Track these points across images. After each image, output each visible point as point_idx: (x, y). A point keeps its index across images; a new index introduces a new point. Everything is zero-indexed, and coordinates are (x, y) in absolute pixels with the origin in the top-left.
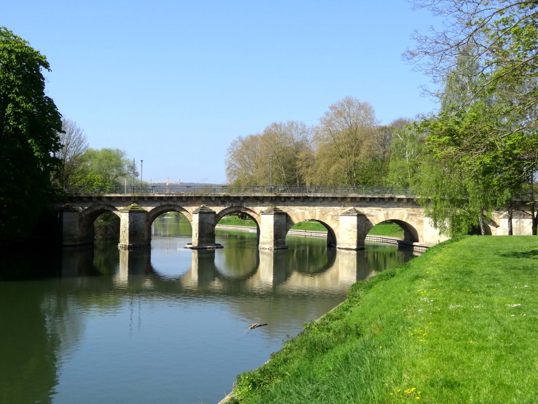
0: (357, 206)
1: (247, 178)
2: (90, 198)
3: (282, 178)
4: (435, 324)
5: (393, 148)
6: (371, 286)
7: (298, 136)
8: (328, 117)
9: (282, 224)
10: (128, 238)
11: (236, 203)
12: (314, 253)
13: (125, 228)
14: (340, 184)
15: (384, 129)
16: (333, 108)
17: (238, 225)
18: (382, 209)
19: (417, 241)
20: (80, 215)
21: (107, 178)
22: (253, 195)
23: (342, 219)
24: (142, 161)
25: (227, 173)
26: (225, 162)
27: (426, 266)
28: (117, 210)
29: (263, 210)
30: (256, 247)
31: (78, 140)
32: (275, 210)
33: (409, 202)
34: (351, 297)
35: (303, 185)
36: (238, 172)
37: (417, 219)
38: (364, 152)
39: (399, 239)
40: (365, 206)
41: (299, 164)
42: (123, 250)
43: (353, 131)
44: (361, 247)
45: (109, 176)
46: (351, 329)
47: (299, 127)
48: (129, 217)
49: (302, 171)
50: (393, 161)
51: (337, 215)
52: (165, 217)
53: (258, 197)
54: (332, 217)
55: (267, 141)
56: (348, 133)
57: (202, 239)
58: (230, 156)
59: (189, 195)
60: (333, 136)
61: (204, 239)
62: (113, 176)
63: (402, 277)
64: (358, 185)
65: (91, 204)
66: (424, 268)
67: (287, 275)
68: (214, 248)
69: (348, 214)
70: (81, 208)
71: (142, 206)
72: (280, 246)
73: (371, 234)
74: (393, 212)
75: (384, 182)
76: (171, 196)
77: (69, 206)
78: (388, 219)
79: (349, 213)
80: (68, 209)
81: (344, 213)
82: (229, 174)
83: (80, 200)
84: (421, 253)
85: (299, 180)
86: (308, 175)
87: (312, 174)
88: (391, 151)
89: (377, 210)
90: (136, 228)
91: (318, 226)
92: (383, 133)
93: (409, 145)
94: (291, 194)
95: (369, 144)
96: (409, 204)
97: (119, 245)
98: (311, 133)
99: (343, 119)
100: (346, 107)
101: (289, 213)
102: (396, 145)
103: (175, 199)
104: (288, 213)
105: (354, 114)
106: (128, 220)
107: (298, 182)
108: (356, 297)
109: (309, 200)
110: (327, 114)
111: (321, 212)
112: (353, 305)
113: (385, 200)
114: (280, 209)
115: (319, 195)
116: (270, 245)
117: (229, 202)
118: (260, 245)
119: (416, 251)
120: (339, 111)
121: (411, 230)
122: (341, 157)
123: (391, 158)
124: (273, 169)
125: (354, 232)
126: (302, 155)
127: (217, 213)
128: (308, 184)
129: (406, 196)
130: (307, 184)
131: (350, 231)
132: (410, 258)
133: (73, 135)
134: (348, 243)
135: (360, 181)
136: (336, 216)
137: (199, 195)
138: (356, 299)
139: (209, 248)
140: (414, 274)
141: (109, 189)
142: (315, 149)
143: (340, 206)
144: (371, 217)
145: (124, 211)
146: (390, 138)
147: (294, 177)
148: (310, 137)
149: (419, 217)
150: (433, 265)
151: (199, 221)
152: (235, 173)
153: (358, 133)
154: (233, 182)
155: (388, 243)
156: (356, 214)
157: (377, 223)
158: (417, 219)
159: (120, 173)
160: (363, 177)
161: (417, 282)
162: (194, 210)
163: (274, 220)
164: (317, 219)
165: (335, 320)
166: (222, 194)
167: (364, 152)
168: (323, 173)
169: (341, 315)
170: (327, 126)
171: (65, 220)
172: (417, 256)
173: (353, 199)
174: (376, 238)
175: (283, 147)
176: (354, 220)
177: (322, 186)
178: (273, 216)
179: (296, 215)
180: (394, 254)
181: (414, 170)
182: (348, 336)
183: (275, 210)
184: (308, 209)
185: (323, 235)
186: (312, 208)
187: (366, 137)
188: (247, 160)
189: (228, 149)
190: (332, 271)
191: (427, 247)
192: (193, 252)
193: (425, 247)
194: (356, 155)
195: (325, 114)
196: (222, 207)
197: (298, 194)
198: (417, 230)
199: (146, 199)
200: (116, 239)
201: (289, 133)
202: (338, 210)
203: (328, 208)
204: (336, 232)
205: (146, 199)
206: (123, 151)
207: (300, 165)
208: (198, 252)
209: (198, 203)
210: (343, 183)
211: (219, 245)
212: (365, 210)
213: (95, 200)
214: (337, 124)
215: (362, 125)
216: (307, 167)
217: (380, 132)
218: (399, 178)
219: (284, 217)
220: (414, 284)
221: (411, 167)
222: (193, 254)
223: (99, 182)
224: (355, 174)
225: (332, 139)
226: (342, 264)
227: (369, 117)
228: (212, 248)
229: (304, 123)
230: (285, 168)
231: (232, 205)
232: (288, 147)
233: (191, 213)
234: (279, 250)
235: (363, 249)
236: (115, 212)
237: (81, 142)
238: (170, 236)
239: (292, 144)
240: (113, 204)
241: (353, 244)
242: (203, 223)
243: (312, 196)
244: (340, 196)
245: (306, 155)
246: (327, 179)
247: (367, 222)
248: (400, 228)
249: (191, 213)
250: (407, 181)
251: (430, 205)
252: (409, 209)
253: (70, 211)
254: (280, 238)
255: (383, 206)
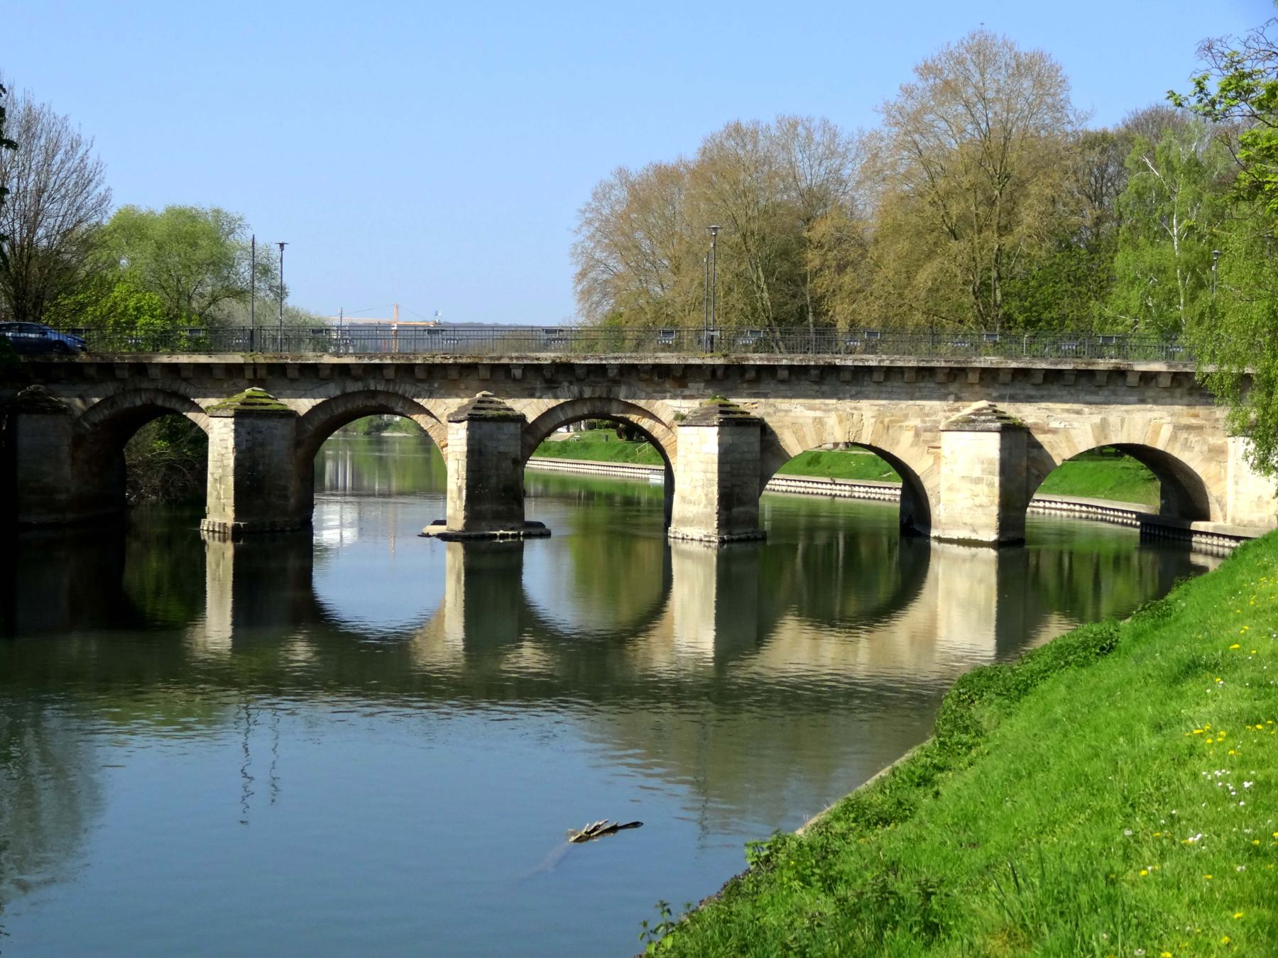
0: (1001, 398)
1: (645, 306)
2: (107, 370)
3: (759, 305)
4: (1260, 923)
5: (1127, 205)
6: (1028, 686)
7: (811, 167)
8: (910, 102)
9: (749, 456)
10: (232, 501)
11: (593, 385)
12: (864, 550)
13: (224, 467)
14: (950, 326)
15: (1100, 142)
16: (927, 70)
17: (612, 459)
18: (1086, 409)
19: (1205, 517)
20: (77, 423)
21: (183, 303)
22: (650, 361)
23: (950, 441)
24: (282, 245)
25: (579, 288)
26: (573, 255)
27: (1231, 616)
28: (198, 409)
29: (685, 412)
30: (661, 534)
31: (74, 176)
32: (725, 409)
33: (1180, 385)
34: (948, 727)
35: (826, 335)
36: (616, 287)
37: (1205, 442)
38: (1030, 220)
39: (1143, 509)
40: (1029, 399)
41: (813, 259)
42: (217, 542)
43: (993, 148)
44: (1012, 535)
45: (190, 298)
46: (901, 906)
47: (817, 137)
48: (236, 431)
49: (822, 284)
50: (1129, 249)
51: (934, 429)
52: (385, 434)
53: (669, 366)
54: (917, 435)
55: (711, 184)
56: (979, 155)
57: (477, 508)
58: (588, 234)
59: (438, 360)
60: (926, 168)
61: (486, 507)
62: (202, 296)
63: (1139, 660)
64: (1010, 328)
65: (110, 388)
66: (1221, 627)
67: (763, 632)
68: (518, 535)
69: (968, 424)
70: (78, 402)
71: (280, 395)
72: (739, 532)
73: (1049, 490)
74: (1123, 421)
75: (1096, 322)
76: (377, 361)
77: (39, 394)
78: (1104, 443)
79: (974, 421)
80: (35, 405)
81: (956, 422)
82: (586, 294)
83: (77, 375)
84: (1217, 556)
85: (815, 314)
86: (844, 294)
87: (858, 292)
88: (1121, 214)
89: (1068, 411)
90: (260, 467)
91: (877, 465)
92: (1094, 156)
93: (1183, 192)
94: (780, 356)
95: (1048, 191)
96: (1178, 392)
97: (205, 524)
98: (857, 155)
99: (961, 109)
100: (972, 67)
101: (771, 422)
102: (1140, 195)
103: (390, 374)
104: (767, 420)
105: (998, 92)
106: (231, 443)
107: (811, 319)
108: (966, 730)
109: (838, 377)
110: (908, 92)
111: (879, 418)
112: (952, 762)
113: (1098, 377)
114: (742, 408)
115: (872, 361)
116: (707, 525)
117: (571, 383)
118: (672, 529)
119: (1200, 552)
120: (947, 83)
121: (1180, 477)
122: (954, 235)
123: (1121, 238)
124: (729, 276)
125: (991, 485)
126: (821, 230)
127: (531, 418)
128: (842, 325)
129: (1170, 366)
130: (839, 325)
131: (978, 481)
132: (1177, 580)
133: (58, 158)
134: (968, 521)
135: (1016, 315)
136: (930, 431)
137: (469, 361)
138: (965, 738)
139: (502, 536)
140: (1182, 651)
141: (189, 339)
142: (869, 210)
143: (943, 397)
144: (1050, 436)
145: (218, 413)
146: (1119, 172)
147: (798, 302)
148: (850, 171)
149: (1213, 435)
150: (1256, 613)
151: (468, 445)
152: (603, 288)
153: (1012, 157)
154: (598, 319)
155: (1105, 521)
156: (998, 424)
157: (1068, 455)
158: (1205, 442)
159: (227, 289)
160: (1027, 304)
161: (1190, 686)
162: (453, 409)
163: (720, 445)
164: (865, 441)
165: (876, 824)
166: (546, 357)
167: (1028, 218)
168: (891, 289)
169: (900, 804)
170: (907, 133)
171: (24, 442)
172: (1202, 570)
173: (989, 376)
174: (1065, 506)
175: (762, 202)
176: (989, 445)
177: (890, 332)
178: (716, 429)
179: (796, 428)
180: (1128, 559)
181: (1199, 279)
182: (888, 933)
183: (725, 409)
184: (837, 410)
185: (889, 493)
186: (847, 405)
187: (1037, 169)
188: (646, 245)
189: (584, 212)
190: (915, 615)
191: (1237, 539)
192: (450, 549)
193: (1231, 537)
194: (1004, 230)
195: (899, 92)
196: (546, 400)
197: (801, 356)
198: (1204, 479)
199: (292, 373)
200: (198, 505)
201: (782, 156)
202: (935, 413)
203: (904, 404)
204: (928, 485)
205: (292, 373)
206: (237, 217)
207: (817, 262)
208: (465, 548)
209: (467, 388)
210: (961, 322)
211: (540, 525)
212: (1027, 413)
213: (126, 374)
214: (943, 125)
215: (1026, 128)
216: (841, 269)
217: (1087, 152)
218: (1147, 307)
219: (753, 437)
220: (1181, 695)
221: (1190, 268)
222: (449, 556)
223: (153, 316)
224: (998, 293)
225: (925, 175)
226: (949, 593)
227: (1049, 100)
228: (513, 536)
229: (832, 124)
230: (769, 273)
231: (581, 393)
232: (779, 205)
233: (444, 420)
234: (735, 546)
235: (1020, 542)
236: (191, 416)
237: (84, 184)
238: (401, 494)
239: (794, 194)
240: (183, 388)
241: (987, 526)
242: (480, 452)
243: (849, 363)
244: (943, 364)
245: (839, 230)
246: (905, 308)
247: (1035, 452)
248: (1146, 473)
249: (444, 420)
250: (1173, 315)
251: (1249, 394)
252: (1177, 408)
253: (43, 411)
254: (741, 503)
255: (1088, 398)
